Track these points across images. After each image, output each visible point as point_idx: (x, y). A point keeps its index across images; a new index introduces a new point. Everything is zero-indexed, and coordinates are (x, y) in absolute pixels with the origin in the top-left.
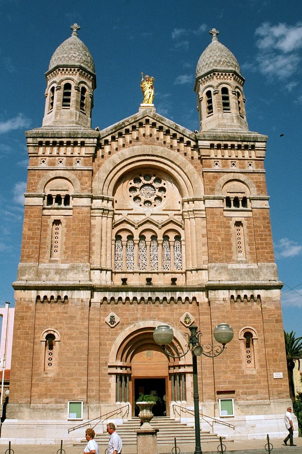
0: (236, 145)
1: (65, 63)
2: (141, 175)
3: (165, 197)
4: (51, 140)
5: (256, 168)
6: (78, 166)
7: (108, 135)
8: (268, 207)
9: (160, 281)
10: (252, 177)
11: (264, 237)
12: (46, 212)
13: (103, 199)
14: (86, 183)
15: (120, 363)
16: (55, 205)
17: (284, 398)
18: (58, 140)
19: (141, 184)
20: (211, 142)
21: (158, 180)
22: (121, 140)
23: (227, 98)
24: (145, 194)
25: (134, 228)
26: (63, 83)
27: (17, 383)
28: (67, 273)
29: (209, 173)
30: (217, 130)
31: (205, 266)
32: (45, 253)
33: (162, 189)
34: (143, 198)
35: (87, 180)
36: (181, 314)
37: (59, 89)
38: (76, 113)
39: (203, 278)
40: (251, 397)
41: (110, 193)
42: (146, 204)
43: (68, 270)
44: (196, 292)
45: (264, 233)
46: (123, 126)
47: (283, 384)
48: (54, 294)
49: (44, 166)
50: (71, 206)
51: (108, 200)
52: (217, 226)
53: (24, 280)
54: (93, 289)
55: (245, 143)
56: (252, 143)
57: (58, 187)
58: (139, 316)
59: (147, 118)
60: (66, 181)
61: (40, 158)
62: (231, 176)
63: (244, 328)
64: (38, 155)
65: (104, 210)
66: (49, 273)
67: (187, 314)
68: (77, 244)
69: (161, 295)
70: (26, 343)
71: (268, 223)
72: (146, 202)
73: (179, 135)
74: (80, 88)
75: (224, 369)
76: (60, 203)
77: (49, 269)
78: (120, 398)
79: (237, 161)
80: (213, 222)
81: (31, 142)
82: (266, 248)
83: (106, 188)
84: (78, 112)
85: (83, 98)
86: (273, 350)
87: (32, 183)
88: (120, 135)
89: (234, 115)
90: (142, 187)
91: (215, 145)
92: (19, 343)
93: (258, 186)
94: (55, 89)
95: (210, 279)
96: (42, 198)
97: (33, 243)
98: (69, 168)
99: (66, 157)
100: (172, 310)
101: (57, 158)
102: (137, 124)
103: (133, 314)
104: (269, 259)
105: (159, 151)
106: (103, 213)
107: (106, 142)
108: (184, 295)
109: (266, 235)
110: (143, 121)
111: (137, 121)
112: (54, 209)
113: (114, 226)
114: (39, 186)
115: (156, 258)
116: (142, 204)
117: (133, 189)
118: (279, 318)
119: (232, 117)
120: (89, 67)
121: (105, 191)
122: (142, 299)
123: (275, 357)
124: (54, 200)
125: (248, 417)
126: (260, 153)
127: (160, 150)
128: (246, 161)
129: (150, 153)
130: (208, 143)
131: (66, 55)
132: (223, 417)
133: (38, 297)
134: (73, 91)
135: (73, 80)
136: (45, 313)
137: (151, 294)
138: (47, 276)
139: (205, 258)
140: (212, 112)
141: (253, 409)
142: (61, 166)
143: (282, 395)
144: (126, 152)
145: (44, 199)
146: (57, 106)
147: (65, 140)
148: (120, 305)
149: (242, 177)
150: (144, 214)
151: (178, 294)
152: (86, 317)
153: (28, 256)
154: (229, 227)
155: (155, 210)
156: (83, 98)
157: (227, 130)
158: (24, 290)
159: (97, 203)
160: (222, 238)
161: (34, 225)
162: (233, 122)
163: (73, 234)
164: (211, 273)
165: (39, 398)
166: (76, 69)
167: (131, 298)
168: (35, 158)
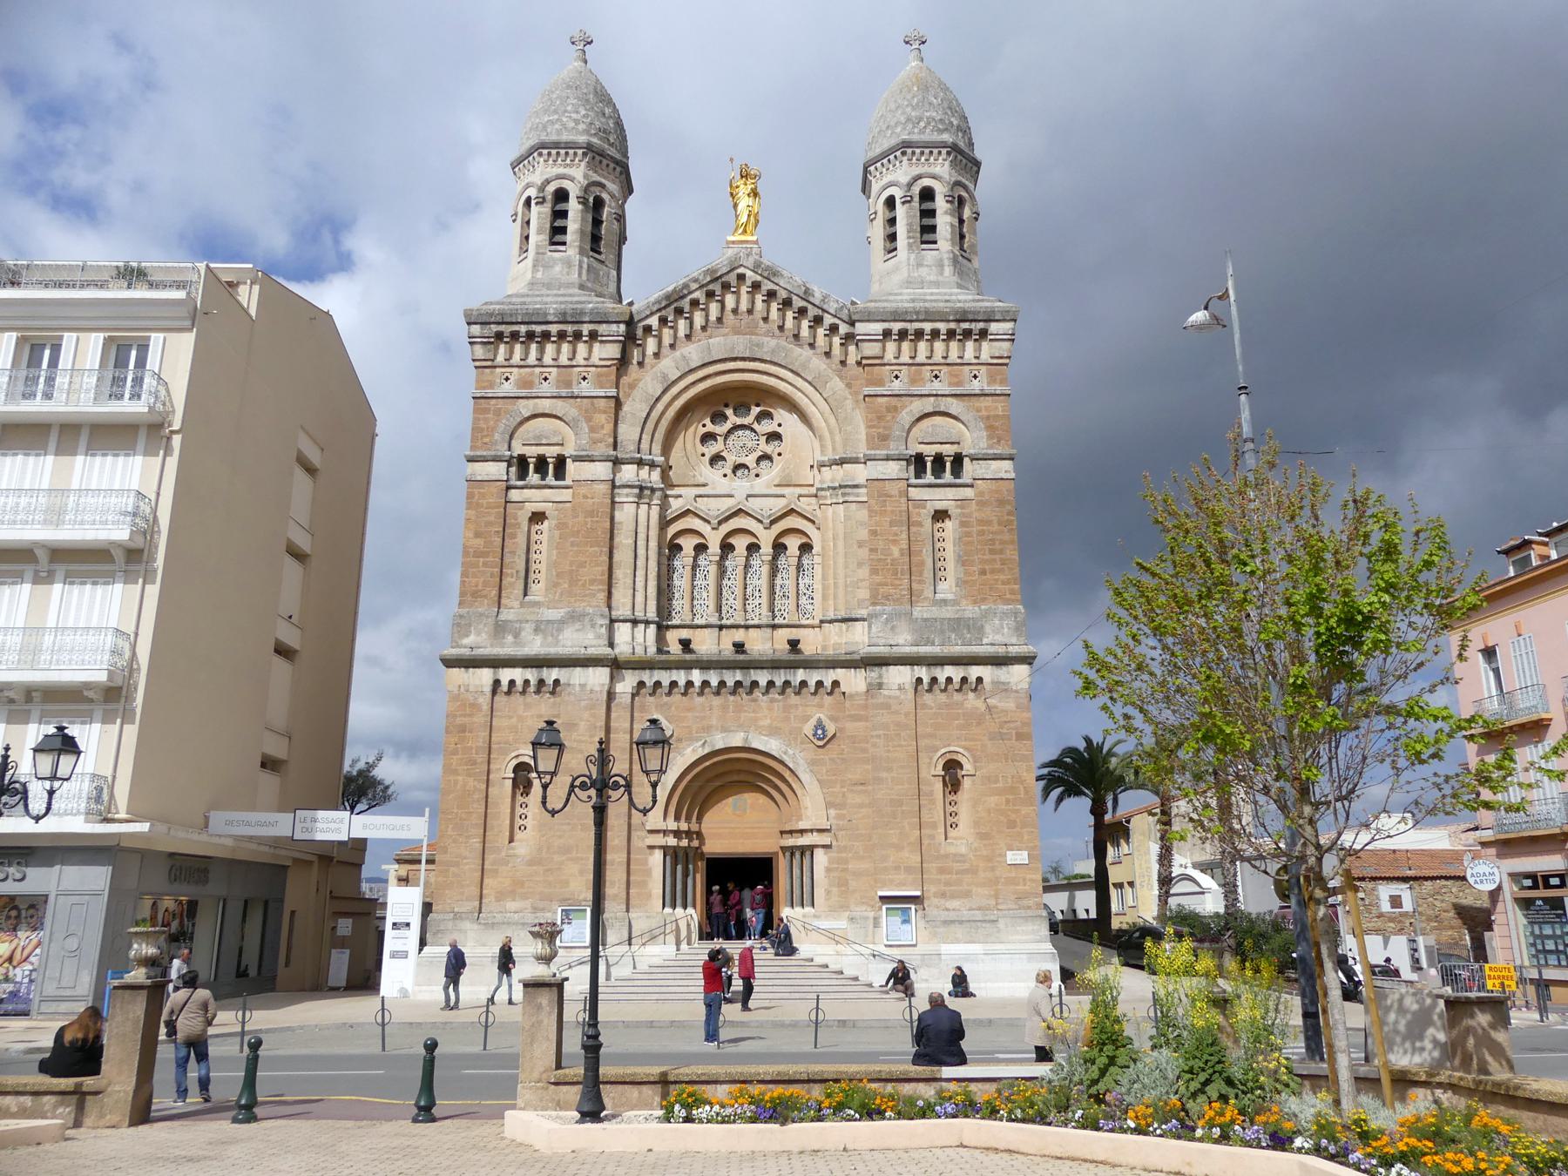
0: (943, 331)
1: (554, 138)
2: (726, 406)
3: (780, 454)
4: (523, 329)
5: (989, 384)
6: (586, 388)
7: (652, 314)
8: (1013, 475)
9: (760, 644)
10: (977, 404)
11: (997, 546)
12: (514, 495)
13: (640, 463)
14: (602, 427)
15: (672, 825)
16: (533, 478)
17: (1029, 908)
18: (538, 329)
19: (728, 425)
20: (886, 325)
21: (765, 415)
22: (682, 325)
23: (931, 213)
24: (741, 448)
25: (708, 528)
26: (551, 188)
27: (452, 869)
28: (560, 630)
29: (880, 400)
30: (901, 294)
31: (863, 613)
32: (512, 584)
33: (774, 437)
34: (732, 459)
35: (604, 421)
36: (806, 719)
37: (542, 203)
38: (581, 262)
39: (858, 639)
40: (955, 904)
41: (657, 448)
42: (739, 473)
43: (562, 622)
44: (839, 670)
46: (685, 292)
47: (1028, 876)
48: (531, 675)
49: (508, 388)
50: (568, 482)
51: (652, 465)
52: (892, 523)
54: (616, 666)
55: (966, 325)
56: (981, 325)
57: (539, 437)
58: (714, 722)
59: (741, 270)
60: (558, 422)
61: (498, 370)
62: (928, 405)
63: (943, 751)
64: (495, 363)
65: (641, 488)
66: (521, 629)
67: (819, 719)
68: (582, 564)
69: (762, 677)
70: (471, 783)
71: (1009, 514)
72: (738, 467)
73: (812, 312)
74: (591, 200)
75: (895, 840)
76: (544, 476)
77: (521, 622)
78: (673, 898)
79: (945, 369)
81: (478, 334)
82: (1001, 571)
83: (646, 437)
84: (585, 260)
85: (597, 222)
86: (1008, 801)
87: (482, 430)
88: (679, 312)
89: (946, 256)
90: (730, 432)
91: (895, 331)
92: (456, 782)
93: (990, 428)
94: (533, 202)
95: (874, 641)
96: (505, 464)
97: (485, 564)
98: (564, 392)
99: (558, 366)
100: (787, 709)
101: (538, 370)
102: (717, 287)
103: (703, 718)
104: (1008, 596)
105: (765, 350)
106: (640, 496)
107: (648, 329)
108: (813, 677)
109: (1002, 542)
110: (732, 278)
111: (717, 279)
112: (532, 487)
113: (664, 523)
114: (497, 436)
115: (757, 594)
116: (729, 471)
117: (708, 437)
118: (1025, 730)
119: (941, 260)
120: (612, 145)
121: (645, 445)
122: (722, 684)
123: (1013, 816)
124: (531, 466)
125: (946, 948)
126: (1000, 348)
127: (769, 344)
128: (967, 368)
129: (747, 355)
130: (878, 328)
131: (556, 117)
132: (890, 946)
133: (497, 683)
134: (574, 207)
135: (572, 179)
136: (511, 717)
137: (744, 675)
138: (515, 637)
139: (864, 593)
140: (896, 249)
141: (959, 931)
142: (546, 388)
143: (1025, 902)
144: (693, 353)
145: (509, 466)
146: (538, 246)
147: (554, 329)
148: (676, 697)
149: (954, 406)
150: (732, 496)
151: (800, 675)
152: (598, 724)
153: (476, 592)
154: (920, 524)
155: (759, 486)
156: (597, 222)
157: (925, 294)
158: (467, 667)
159: (628, 473)
160: (901, 550)
162: (942, 274)
163: (573, 544)
164: (874, 629)
165: (498, 900)
166: (580, 152)
167: (697, 684)
168: (487, 370)
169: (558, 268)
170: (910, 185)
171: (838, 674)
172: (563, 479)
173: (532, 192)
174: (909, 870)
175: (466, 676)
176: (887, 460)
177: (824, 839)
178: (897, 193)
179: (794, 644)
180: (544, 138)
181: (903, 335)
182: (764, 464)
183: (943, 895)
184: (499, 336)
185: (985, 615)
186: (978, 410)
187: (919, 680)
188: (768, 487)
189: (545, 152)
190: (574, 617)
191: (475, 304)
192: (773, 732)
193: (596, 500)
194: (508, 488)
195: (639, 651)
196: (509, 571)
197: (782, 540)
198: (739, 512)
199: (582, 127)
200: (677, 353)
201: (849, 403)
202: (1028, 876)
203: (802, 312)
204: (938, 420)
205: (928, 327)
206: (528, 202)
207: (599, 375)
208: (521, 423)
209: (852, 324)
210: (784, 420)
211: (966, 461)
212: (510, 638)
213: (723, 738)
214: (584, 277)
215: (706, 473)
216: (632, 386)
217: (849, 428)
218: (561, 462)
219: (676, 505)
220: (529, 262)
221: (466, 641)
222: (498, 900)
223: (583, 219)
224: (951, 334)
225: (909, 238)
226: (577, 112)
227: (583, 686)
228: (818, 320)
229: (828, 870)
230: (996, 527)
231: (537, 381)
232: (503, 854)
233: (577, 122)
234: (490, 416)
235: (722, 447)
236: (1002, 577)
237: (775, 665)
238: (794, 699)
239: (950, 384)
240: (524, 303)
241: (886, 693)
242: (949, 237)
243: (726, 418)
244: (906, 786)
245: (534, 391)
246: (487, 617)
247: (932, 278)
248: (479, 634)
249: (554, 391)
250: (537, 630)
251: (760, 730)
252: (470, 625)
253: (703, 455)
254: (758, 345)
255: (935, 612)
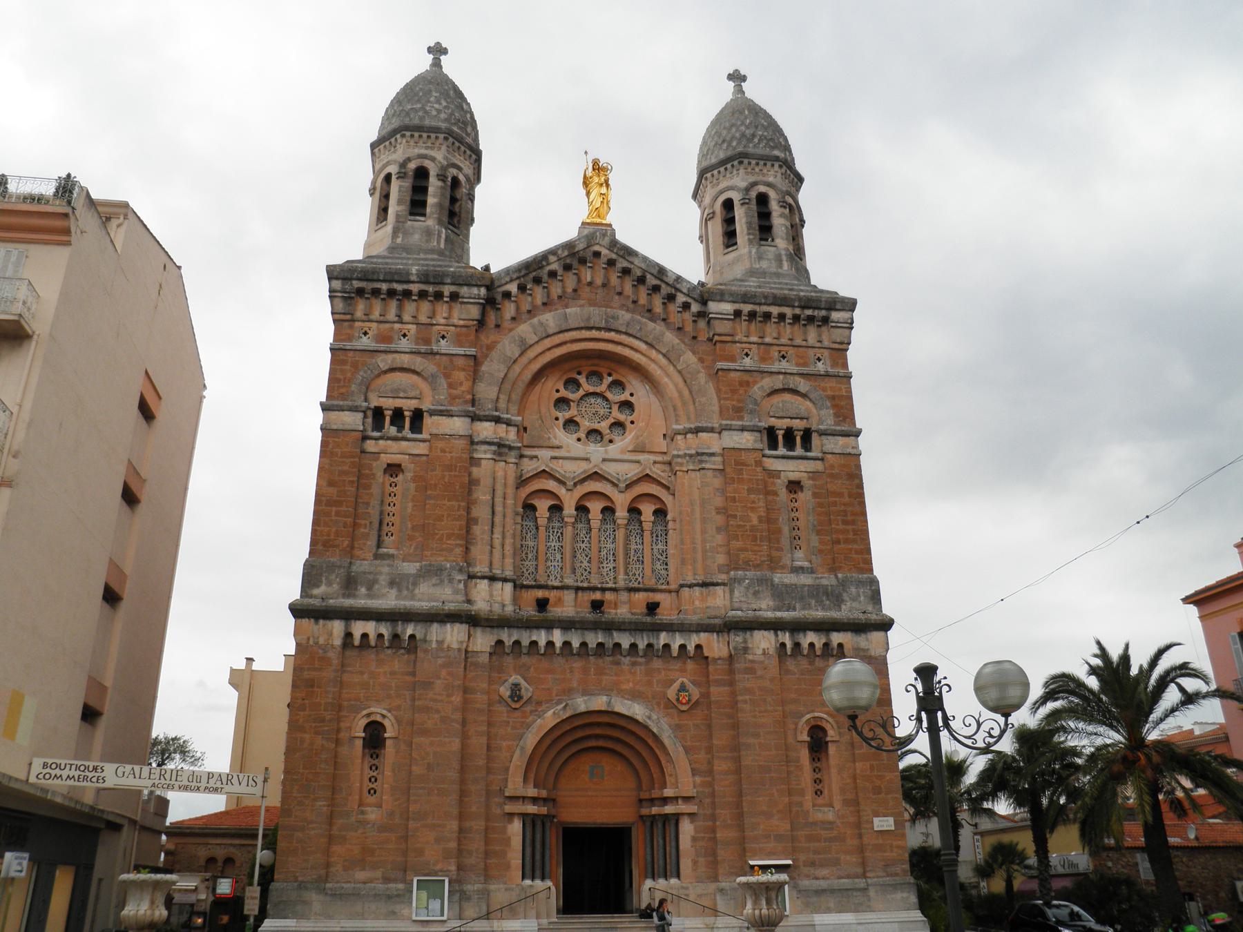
1: (416, 122)
2: (579, 373)
3: (632, 422)
4: (384, 287)
5: (832, 366)
6: (444, 347)
7: (511, 281)
11: (849, 518)
12: (370, 446)
15: (532, 792)
17: (897, 875)
19: (581, 392)
20: (737, 306)
21: (618, 384)
26: (412, 166)
28: (415, 584)
31: (721, 577)
34: (586, 424)
39: (719, 602)
40: (824, 872)
42: (592, 438)
44: (702, 634)
45: (850, 509)
47: (895, 843)
49: (365, 342)
50: (424, 436)
52: (750, 491)
53: (316, 597)
55: (809, 312)
57: (398, 390)
58: (575, 684)
60: (415, 377)
62: (778, 382)
65: (500, 445)
67: (682, 683)
69: (625, 641)
70: (319, 741)
73: (665, 290)
76: (401, 428)
78: (533, 869)
79: (791, 351)
80: (741, 481)
86: (872, 767)
88: (537, 281)
94: (394, 178)
97: (337, 514)
98: (423, 348)
101: (397, 326)
107: (507, 295)
108: (677, 641)
113: (522, 482)
114: (354, 387)
116: (583, 436)
117: (562, 402)
119: (780, 255)
121: (502, 405)
130: (727, 307)
131: (419, 106)
135: (433, 159)
136: (362, 673)
139: (721, 559)
140: (736, 244)
142: (404, 344)
146: (398, 216)
147: (415, 288)
149: (803, 386)
154: (775, 494)
155: (613, 450)
159: (486, 430)
160: (760, 518)
161: (342, 473)
164: (736, 593)
165: (346, 869)
167: (558, 644)
169: (417, 237)
170: (747, 190)
171: (702, 638)
172: (421, 432)
173: (393, 169)
174: (779, 838)
175: (316, 628)
176: (742, 430)
177: (692, 808)
178: (736, 197)
179: (652, 608)
180: (407, 121)
181: (752, 315)
182: (617, 430)
183: (813, 864)
184: (360, 292)
185: (843, 584)
186: (824, 390)
187: (783, 645)
188: (622, 452)
189: (408, 134)
190: (432, 572)
191: (339, 260)
192: (635, 696)
193: (454, 454)
194: (365, 438)
195: (497, 608)
196: (363, 522)
197: (582, 503)
198: (596, 476)
199: (443, 116)
200: (535, 320)
201: (702, 377)
202: (895, 843)
203: (656, 289)
204: (787, 397)
205: (775, 310)
206: (388, 178)
207: (458, 335)
208: (379, 376)
209: (704, 303)
210: (638, 392)
211: (814, 436)
212: (363, 590)
213: (585, 702)
214: (442, 246)
215: (561, 436)
216: (490, 348)
217: (703, 400)
218: (418, 415)
219: (529, 467)
220: (389, 228)
221: (316, 592)
222: (346, 869)
223: (443, 195)
224: (796, 318)
225: (749, 234)
226: (440, 104)
227: (440, 643)
228: (671, 298)
229: (694, 839)
230: (847, 499)
231: (396, 337)
232: (353, 819)
233: (439, 111)
234: (348, 367)
235: (575, 413)
236: (855, 546)
237: (635, 627)
238: (657, 663)
239: (798, 365)
240: (387, 264)
241: (750, 657)
242: (784, 236)
243: (579, 385)
244: (774, 752)
245: (393, 346)
246: (340, 567)
247: (774, 270)
248: (329, 584)
249: (414, 347)
250: (392, 583)
251: (622, 693)
252: (321, 575)
253: (557, 419)
254: (613, 318)
255: (790, 579)
